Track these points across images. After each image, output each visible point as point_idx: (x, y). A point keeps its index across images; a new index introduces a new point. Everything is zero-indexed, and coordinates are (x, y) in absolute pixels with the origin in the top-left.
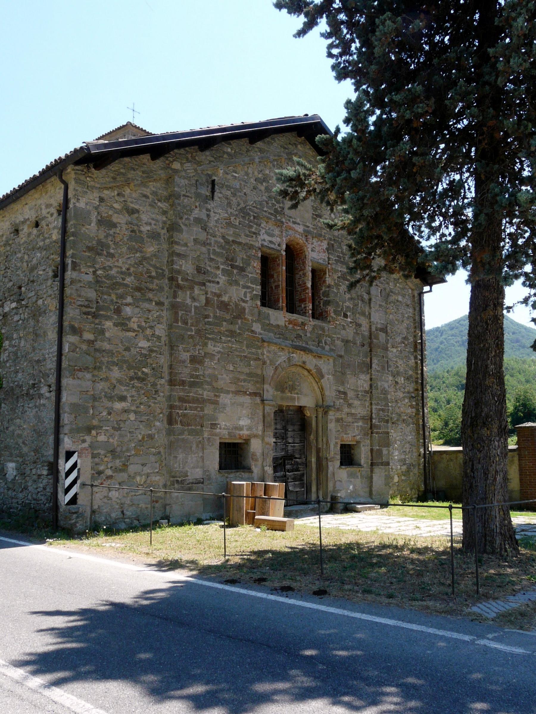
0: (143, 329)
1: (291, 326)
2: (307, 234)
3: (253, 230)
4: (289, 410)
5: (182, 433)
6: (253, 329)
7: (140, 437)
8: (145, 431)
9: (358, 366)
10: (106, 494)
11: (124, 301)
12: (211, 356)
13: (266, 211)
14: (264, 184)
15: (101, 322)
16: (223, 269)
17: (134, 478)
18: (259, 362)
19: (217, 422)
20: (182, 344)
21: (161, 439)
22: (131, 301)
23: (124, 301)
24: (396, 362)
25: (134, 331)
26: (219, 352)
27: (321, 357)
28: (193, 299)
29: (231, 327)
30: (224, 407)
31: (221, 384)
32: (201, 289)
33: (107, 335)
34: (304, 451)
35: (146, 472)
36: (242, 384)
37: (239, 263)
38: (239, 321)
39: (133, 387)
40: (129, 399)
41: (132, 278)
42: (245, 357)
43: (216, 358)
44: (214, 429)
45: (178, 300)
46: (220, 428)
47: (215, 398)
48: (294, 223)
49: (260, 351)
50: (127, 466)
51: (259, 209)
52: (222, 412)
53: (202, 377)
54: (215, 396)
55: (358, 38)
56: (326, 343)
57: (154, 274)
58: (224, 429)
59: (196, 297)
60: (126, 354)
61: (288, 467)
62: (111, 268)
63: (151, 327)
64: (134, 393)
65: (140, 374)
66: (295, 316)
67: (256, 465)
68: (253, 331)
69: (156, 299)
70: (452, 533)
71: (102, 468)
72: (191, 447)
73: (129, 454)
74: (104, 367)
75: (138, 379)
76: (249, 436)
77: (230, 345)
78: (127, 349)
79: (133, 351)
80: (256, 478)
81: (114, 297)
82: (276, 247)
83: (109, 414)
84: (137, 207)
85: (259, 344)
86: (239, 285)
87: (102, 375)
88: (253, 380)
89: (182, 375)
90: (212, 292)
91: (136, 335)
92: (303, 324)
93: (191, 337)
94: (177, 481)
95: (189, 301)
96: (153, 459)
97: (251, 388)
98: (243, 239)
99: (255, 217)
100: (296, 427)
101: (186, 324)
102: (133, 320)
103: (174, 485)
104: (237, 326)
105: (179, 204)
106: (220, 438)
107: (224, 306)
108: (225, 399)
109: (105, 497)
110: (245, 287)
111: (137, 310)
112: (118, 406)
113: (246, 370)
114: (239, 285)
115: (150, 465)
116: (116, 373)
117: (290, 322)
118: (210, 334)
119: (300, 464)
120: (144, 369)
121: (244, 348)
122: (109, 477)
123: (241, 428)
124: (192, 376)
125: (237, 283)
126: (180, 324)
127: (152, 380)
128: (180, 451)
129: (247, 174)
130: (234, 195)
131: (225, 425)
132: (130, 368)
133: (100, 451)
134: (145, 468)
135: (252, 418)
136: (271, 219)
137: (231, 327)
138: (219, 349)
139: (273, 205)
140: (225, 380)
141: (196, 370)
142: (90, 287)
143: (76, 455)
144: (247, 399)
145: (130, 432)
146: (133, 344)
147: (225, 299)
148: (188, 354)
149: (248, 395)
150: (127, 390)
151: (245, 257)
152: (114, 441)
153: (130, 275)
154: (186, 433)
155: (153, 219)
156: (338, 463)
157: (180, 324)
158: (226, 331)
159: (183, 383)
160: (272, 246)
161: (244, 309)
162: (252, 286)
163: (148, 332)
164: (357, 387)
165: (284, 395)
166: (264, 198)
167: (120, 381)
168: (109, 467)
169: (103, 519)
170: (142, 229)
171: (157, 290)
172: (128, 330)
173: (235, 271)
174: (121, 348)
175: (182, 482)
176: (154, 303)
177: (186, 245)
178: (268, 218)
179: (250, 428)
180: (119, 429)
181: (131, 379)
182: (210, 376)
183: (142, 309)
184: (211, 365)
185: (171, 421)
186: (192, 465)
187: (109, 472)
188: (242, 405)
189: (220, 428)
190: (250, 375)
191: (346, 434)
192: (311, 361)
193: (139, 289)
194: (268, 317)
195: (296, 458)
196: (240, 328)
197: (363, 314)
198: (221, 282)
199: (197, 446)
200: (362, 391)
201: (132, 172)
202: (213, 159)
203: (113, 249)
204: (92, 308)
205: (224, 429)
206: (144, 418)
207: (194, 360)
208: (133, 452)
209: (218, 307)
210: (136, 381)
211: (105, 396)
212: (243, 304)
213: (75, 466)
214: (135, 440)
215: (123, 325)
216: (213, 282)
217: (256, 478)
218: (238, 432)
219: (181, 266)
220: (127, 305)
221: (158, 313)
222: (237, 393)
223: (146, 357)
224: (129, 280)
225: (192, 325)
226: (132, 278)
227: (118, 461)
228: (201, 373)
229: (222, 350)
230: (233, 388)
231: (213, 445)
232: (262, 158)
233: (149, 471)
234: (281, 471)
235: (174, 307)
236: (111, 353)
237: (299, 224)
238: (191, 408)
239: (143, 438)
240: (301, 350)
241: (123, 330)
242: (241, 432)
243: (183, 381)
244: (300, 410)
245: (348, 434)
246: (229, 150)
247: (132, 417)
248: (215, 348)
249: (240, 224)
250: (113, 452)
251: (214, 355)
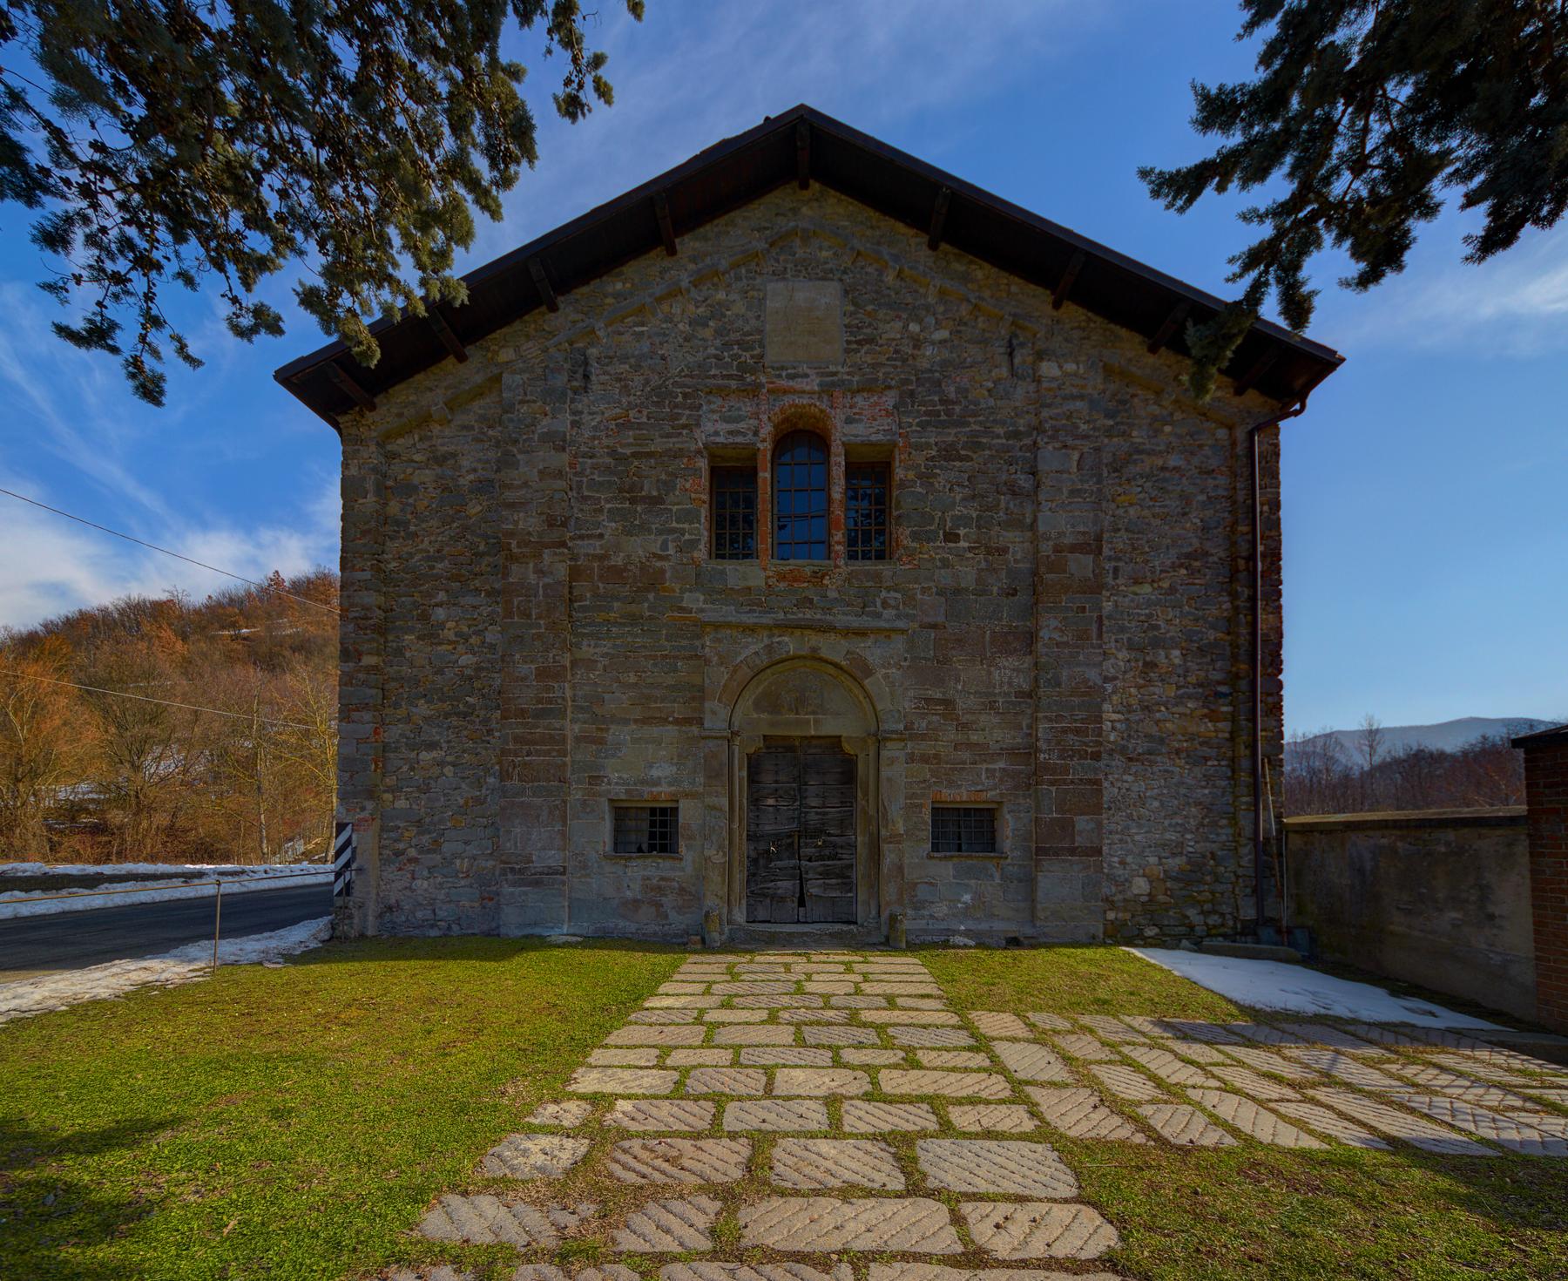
1: (782, 585)
2: (827, 390)
6: (684, 604)
7: (461, 802)
16: (610, 510)
28: (540, 572)
34: (846, 823)
37: (649, 489)
38: (651, 596)
47: (599, 734)
48: (791, 377)
49: (697, 643)
55: (1284, 24)
56: (885, 604)
57: (482, 548)
60: (438, 678)
62: (411, 555)
68: (682, 609)
71: (401, 846)
72: (538, 816)
75: (458, 714)
78: (440, 672)
79: (449, 673)
82: (750, 438)
84: (451, 448)
86: (649, 531)
87: (401, 712)
93: (539, 636)
94: (512, 870)
95: (532, 578)
98: (658, 445)
99: (685, 395)
101: (529, 616)
105: (511, 420)
106: (611, 800)
107: (617, 574)
110: (660, 532)
113: (670, 680)
116: (423, 709)
117: (782, 577)
118: (583, 626)
124: (540, 701)
129: (669, 319)
130: (637, 368)
139: (735, 357)
141: (549, 689)
143: (349, 828)
147: (618, 560)
151: (663, 477)
153: (442, 559)
155: (479, 460)
159: (522, 713)
161: (662, 571)
166: (712, 351)
170: (462, 481)
177: (526, 484)
187: (412, 852)
197: (1013, 523)
201: (429, 394)
202: (581, 316)
207: (542, 674)
212: (658, 564)
213: (348, 843)
215: (431, 635)
216: (589, 537)
218: (646, 789)
219: (516, 523)
237: (806, 376)
238: (538, 753)
239: (466, 803)
245: (960, 786)
246: (619, 286)
250: (419, 823)
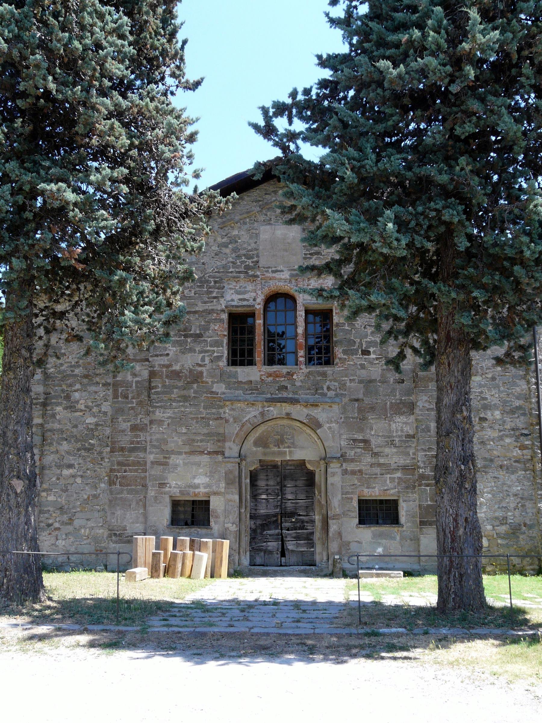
3: (214, 295)
4: (287, 465)
5: (121, 492)
6: (214, 390)
7: (86, 497)
10: (53, 542)
11: (73, 388)
12: (160, 422)
18: (221, 421)
19: (166, 482)
20: (122, 416)
21: (104, 498)
23: (73, 388)
24: (481, 392)
25: (81, 411)
26: (169, 418)
27: (317, 405)
28: (134, 375)
29: (185, 393)
32: (143, 365)
33: (58, 417)
34: (309, 508)
38: (195, 386)
39: (80, 456)
40: (77, 466)
42: (203, 418)
43: (166, 423)
45: (118, 379)
46: (170, 487)
49: (221, 411)
50: (73, 520)
51: (223, 272)
52: (173, 472)
53: (143, 443)
56: (329, 388)
58: (174, 487)
59: (137, 373)
60: (75, 430)
63: (98, 406)
64: (81, 461)
65: (86, 445)
66: (275, 368)
69: (103, 381)
72: (130, 505)
74: (54, 443)
75: (85, 449)
77: (183, 409)
78: (76, 426)
79: (80, 427)
80: (216, 534)
81: (64, 387)
82: (251, 302)
83: (58, 479)
85: (221, 404)
86: (195, 351)
88: (213, 440)
89: (121, 443)
90: (160, 365)
93: (133, 408)
95: (129, 378)
97: (210, 447)
100: (300, 483)
101: (127, 398)
104: (192, 391)
108: (177, 460)
109: (53, 544)
110: (200, 352)
111: (84, 394)
112: (66, 472)
114: (195, 351)
115: (94, 520)
116: (65, 446)
117: (270, 375)
118: (157, 403)
119: (307, 522)
121: (201, 410)
122: (58, 529)
123: (197, 486)
126: (120, 399)
127: (98, 449)
128: (118, 508)
131: (177, 484)
134: (89, 523)
137: (185, 393)
138: (169, 415)
140: (176, 441)
141: (137, 436)
144: (205, 459)
147: (177, 367)
148: (129, 424)
149: (206, 454)
150: (74, 459)
151: (203, 323)
152: (63, 501)
156: (357, 520)
157: (120, 399)
158: (178, 397)
159: (122, 449)
160: (245, 303)
162: (212, 349)
163: (95, 410)
165: (268, 450)
167: (68, 453)
171: (104, 374)
172: (76, 411)
173: (189, 340)
174: (69, 426)
175: (120, 535)
178: (234, 277)
179: (207, 486)
180: (67, 490)
181: (79, 450)
184: (160, 430)
185: (111, 483)
186: (131, 521)
187: (57, 525)
188: (198, 464)
189: (170, 487)
190: (208, 435)
192: (299, 412)
193: (86, 376)
195: (300, 515)
196: (195, 392)
198: (171, 353)
200: (400, 436)
206: (89, 481)
207: (134, 428)
208: (79, 509)
210: (83, 451)
212: (200, 369)
215: (71, 407)
216: (161, 355)
218: (192, 490)
220: (75, 391)
223: (91, 431)
224: (77, 371)
225: (133, 398)
227: (65, 516)
228: (142, 438)
229: (172, 416)
230: (187, 449)
234: (276, 528)
235: (116, 385)
237: (282, 271)
238: (131, 471)
239: (88, 498)
240: (282, 402)
243: (122, 447)
245: (374, 488)
247: (79, 480)
248: (164, 415)
249: (195, 294)
251: (164, 421)
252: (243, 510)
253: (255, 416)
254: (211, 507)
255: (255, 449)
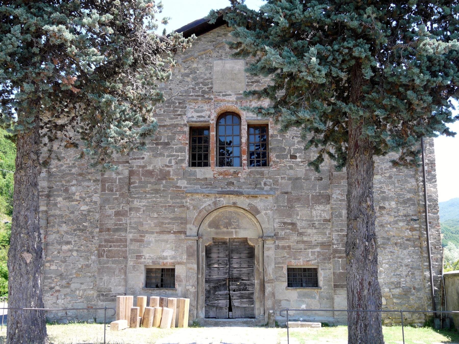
0: (84, 199)
3: (179, 113)
4: (234, 242)
5: (108, 262)
6: (178, 185)
7: (80, 266)
8: (82, 262)
9: (312, 199)
10: (55, 301)
11: (71, 184)
13: (192, 96)
14: (191, 76)
15: (55, 199)
17: (75, 292)
18: (183, 209)
19: (142, 254)
20: (108, 204)
21: (94, 267)
22: (76, 183)
23: (71, 184)
25: (77, 201)
27: (256, 197)
29: (155, 187)
30: (149, 243)
31: (146, 227)
32: (124, 166)
33: (59, 206)
34: (250, 274)
35: (83, 288)
36: (167, 226)
40: (73, 243)
41: (77, 168)
42: (170, 206)
43: (142, 210)
44: (139, 259)
45: (105, 176)
46: (145, 259)
50: (70, 284)
51: (185, 96)
52: (147, 247)
53: (124, 225)
54: (141, 236)
58: (148, 259)
60: (72, 215)
61: (232, 287)
63: (90, 197)
64: (76, 239)
66: (225, 168)
67: (179, 285)
70: (105, 316)
71: (53, 285)
73: (71, 277)
74: (56, 225)
75: (80, 230)
76: (173, 263)
77: (154, 199)
78: (73, 212)
79: (76, 213)
81: (64, 183)
82: (207, 118)
88: (177, 223)
89: (108, 225)
90: (137, 166)
91: (79, 203)
92: (236, 173)
93: (116, 199)
94: (103, 295)
95: (114, 176)
96: (88, 279)
101: (112, 191)
102: (76, 194)
103: (99, 297)
107: (150, 173)
108: (149, 238)
109: (54, 303)
110: (168, 156)
112: (65, 247)
113: (171, 216)
115: (86, 284)
116: (64, 228)
117: (221, 174)
118: (135, 194)
119: (249, 285)
120: (84, 224)
122: (59, 291)
123: (165, 258)
124: (116, 225)
125: (161, 155)
126: (107, 192)
127: (90, 230)
131: (150, 256)
132: (74, 223)
133: (52, 275)
134: (82, 286)
135: (175, 250)
136: (198, 100)
137: (155, 187)
139: (200, 88)
140: (149, 224)
142: (44, 180)
144: (172, 237)
145: (72, 263)
146: (76, 209)
147: (150, 168)
148: (114, 211)
149: (172, 233)
152: (62, 269)
153: (75, 167)
154: (110, 262)
157: (107, 192)
159: (108, 230)
162: (177, 154)
164: (312, 217)
167: (67, 233)
168: (58, 284)
169: (52, 316)
173: (159, 147)
174: (67, 212)
175: (106, 295)
176: (92, 181)
181: (75, 230)
182: (135, 223)
183: (83, 186)
184: (137, 215)
185: (100, 255)
186: (115, 284)
187: (57, 288)
188: (167, 241)
189: (145, 259)
191: (295, 259)
193: (80, 175)
194: (194, 174)
196: (164, 187)
199: (120, 271)
200: (319, 221)
203: (64, 154)
204: (45, 192)
205: (148, 259)
207: (117, 214)
208: (74, 276)
209: (143, 175)
210: (78, 231)
211: (57, 243)
212: (168, 169)
214: (76, 268)
215: (69, 198)
216: (138, 159)
217: (180, 295)
220: (72, 186)
221: (95, 187)
222: (162, 232)
223: (85, 216)
224: (74, 171)
225: (116, 191)
226: (77, 168)
227: (64, 281)
228: (123, 222)
229: (147, 204)
230: (158, 229)
231: (137, 270)
232: (186, 58)
233: (85, 288)
234: (225, 290)
235: (103, 181)
236: (62, 216)
237: (230, 95)
238: (115, 246)
239: (82, 267)
241: (69, 201)
242: (165, 261)
244: (245, 241)
245: (299, 259)
247: (75, 254)
248: (141, 204)
251: (140, 208)
252: (200, 276)
253: (209, 205)
254: (176, 274)
255: (209, 230)
